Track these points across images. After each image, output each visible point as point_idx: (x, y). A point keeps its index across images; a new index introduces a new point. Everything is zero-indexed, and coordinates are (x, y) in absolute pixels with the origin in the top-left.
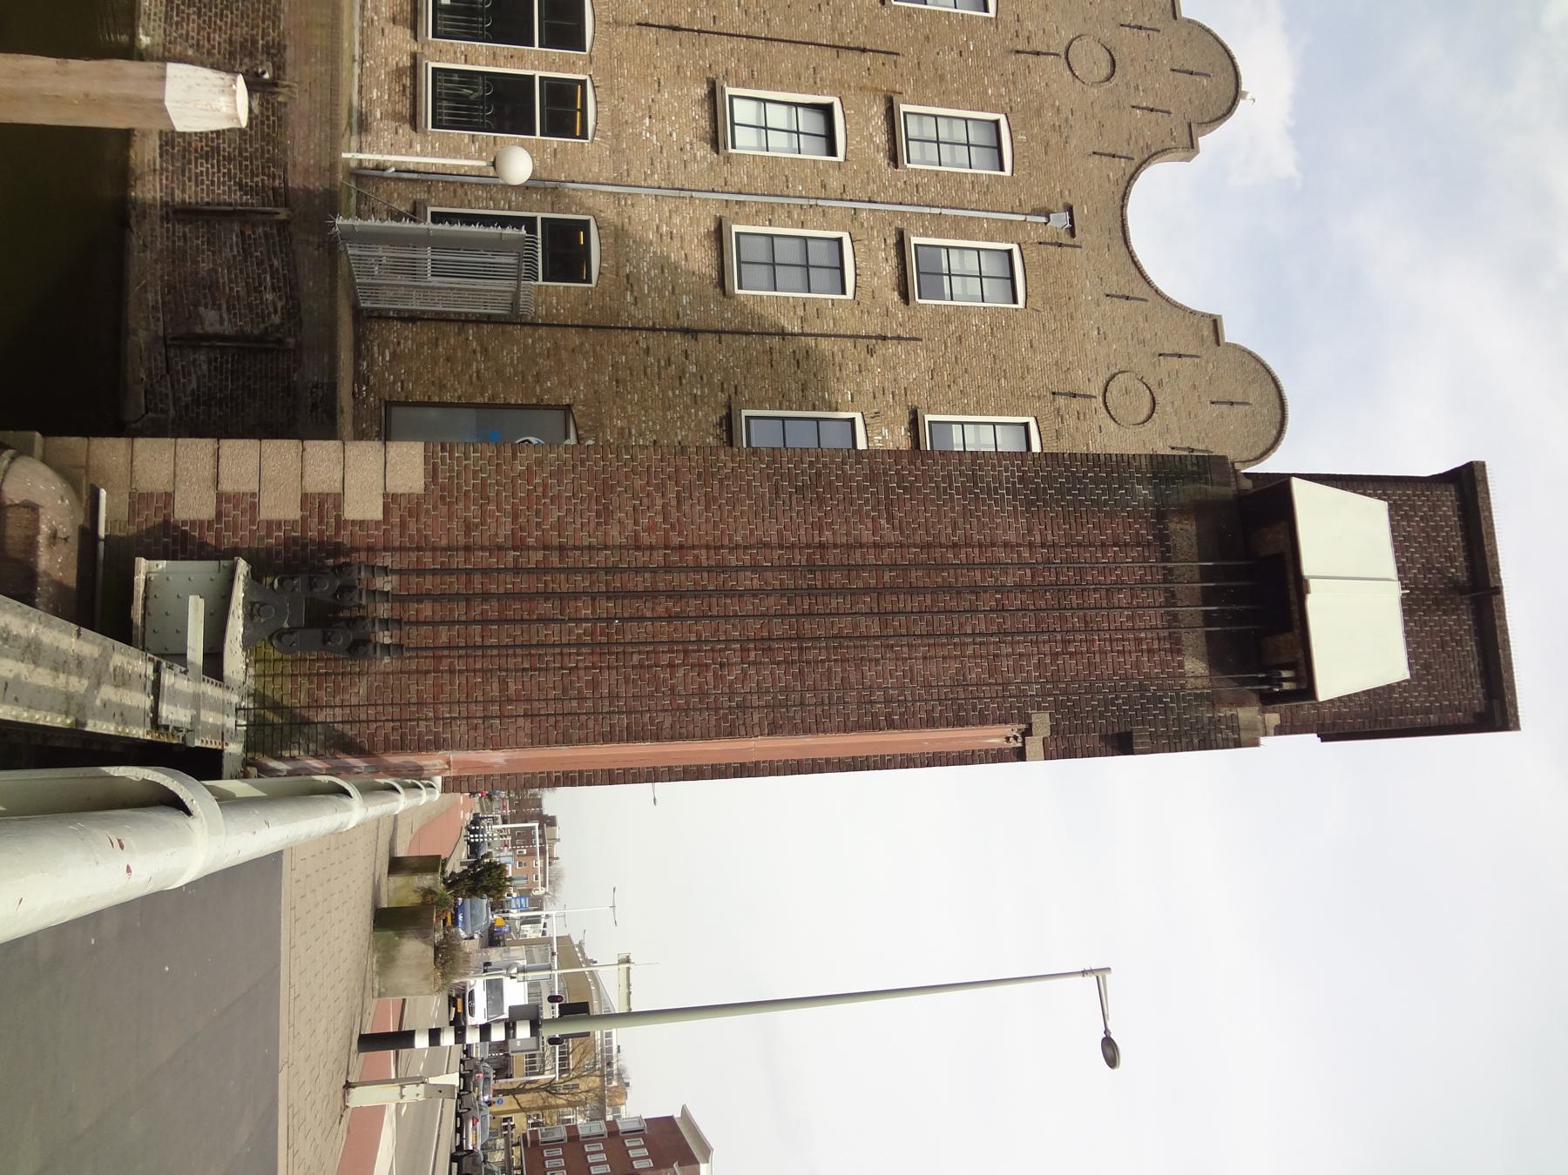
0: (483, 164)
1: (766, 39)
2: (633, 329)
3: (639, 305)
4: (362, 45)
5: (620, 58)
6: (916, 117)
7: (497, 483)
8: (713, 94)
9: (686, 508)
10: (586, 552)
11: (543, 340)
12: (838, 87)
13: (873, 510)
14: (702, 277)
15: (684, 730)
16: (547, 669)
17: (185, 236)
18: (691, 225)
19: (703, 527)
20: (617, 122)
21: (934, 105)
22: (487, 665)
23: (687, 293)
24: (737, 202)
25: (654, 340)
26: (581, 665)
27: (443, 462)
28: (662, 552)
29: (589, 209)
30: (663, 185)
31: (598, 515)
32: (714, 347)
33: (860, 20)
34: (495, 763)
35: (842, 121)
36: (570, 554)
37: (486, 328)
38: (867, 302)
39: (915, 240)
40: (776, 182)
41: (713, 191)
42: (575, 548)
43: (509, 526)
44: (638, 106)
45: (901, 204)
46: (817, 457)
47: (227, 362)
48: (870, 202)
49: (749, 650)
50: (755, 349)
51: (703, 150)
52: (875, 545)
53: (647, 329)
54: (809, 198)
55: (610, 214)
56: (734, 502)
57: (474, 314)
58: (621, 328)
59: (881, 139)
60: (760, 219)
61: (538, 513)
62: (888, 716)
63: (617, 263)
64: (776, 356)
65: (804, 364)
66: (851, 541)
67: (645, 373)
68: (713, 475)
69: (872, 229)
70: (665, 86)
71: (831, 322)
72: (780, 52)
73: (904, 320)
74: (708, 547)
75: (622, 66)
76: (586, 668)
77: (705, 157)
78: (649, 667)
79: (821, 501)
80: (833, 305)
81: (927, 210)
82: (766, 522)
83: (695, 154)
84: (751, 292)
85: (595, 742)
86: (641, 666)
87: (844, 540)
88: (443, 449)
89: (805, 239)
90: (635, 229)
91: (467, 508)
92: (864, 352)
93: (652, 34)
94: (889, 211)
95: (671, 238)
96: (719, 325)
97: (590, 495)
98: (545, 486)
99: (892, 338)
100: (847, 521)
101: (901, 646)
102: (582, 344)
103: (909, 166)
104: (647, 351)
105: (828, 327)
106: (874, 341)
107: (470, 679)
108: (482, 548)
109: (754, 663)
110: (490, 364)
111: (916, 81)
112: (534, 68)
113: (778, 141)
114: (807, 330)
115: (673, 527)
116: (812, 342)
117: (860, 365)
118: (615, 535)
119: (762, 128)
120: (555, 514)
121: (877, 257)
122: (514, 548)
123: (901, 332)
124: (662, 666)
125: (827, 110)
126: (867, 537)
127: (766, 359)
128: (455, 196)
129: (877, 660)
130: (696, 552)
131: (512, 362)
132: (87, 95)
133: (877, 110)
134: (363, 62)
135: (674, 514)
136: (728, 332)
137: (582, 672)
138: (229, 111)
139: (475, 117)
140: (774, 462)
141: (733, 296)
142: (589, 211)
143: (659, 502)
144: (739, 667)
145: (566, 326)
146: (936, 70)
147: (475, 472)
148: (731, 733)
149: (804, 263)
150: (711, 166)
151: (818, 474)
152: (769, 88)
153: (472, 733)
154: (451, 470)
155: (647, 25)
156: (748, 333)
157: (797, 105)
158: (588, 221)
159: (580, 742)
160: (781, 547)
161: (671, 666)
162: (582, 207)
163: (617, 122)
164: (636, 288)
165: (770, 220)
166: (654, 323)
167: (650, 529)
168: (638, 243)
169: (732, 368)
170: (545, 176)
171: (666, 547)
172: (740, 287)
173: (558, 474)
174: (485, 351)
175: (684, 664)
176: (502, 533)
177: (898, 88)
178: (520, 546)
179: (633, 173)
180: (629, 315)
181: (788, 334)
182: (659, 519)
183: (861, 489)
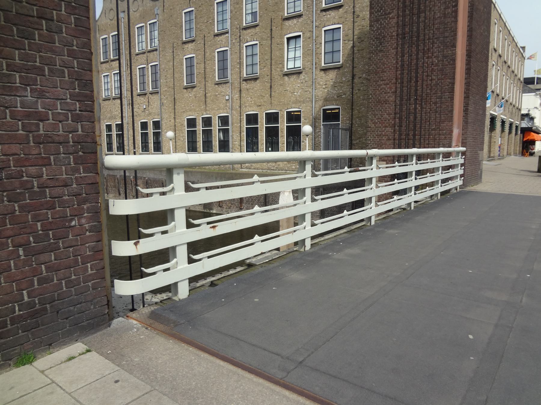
0: (307, 139)
1: (271, 60)
2: (352, 94)
3: (346, 93)
4: (282, 170)
5: (280, 102)
6: (288, 10)
7: (377, 132)
8: (287, 75)
9: (385, 78)
10: (397, 107)
11: (356, 122)
12: (282, 37)
13: (387, 19)
14: (337, 74)
15: (452, 75)
16: (430, 117)
17: (328, 213)
18: (322, 79)
19: (391, 73)
20: (296, 102)
21: (284, 5)
22: (427, 134)
23: (342, 78)
24: (315, 65)
25: (356, 88)
26: (429, 107)
27: (371, 146)
28: (398, 85)
29: (319, 109)
30: (312, 88)
31: (386, 104)
32: (358, 69)
33: (263, 32)
34: (458, 132)
35: (291, 34)
36: (397, 111)
37: (353, 138)
38: (343, 20)
39: (324, 5)
40: (309, 53)
41: (313, 73)
42: (395, 110)
43: (389, 128)
44: (292, 96)
45: (313, 12)
46: (371, 39)
47: (359, 205)
48: (313, 22)
49: (428, 56)
50: (358, 56)
51: (302, 76)
52: (398, 18)
53: (353, 90)
54: (313, 42)
55: (320, 103)
56: (384, 64)
57: (349, 141)
58: (352, 98)
59: (295, 21)
60: (320, 57)
61: (385, 121)
62: (453, 7)
63: (334, 100)
64: (360, 48)
65: (362, 39)
66: (396, 26)
67: (366, 90)
68: (376, 71)
69: (321, 20)
70: (286, 89)
71: (349, 31)
72: (274, 55)
73: (348, 6)
74: (397, 71)
75: (282, 101)
76: (430, 106)
77: (304, 76)
78: (431, 87)
79: (384, 37)
80: (344, 31)
81: (314, 3)
82: (390, 53)
83: (303, 79)
84: (341, 58)
85: (453, 103)
86: (431, 89)
87: (396, 28)
88: (368, 146)
89: (325, 42)
90: (324, 95)
91: (384, 140)
92: (359, 19)
93: (273, 93)
94: (316, 16)
95: (326, 84)
96: (351, 68)
97: (381, 106)
98: (378, 119)
99: (354, 9)
100: (390, 28)
101: (430, 5)
102: (357, 110)
103: (302, 11)
104: (359, 90)
105: (351, 32)
106: (355, 16)
107: (431, 139)
108: (394, 135)
109: (432, 54)
110: (363, 137)
111: (278, 12)
112: (284, 126)
113: (299, 53)
114: (352, 39)
115: (390, 82)
116: (356, 37)
117: (363, 20)
118: (392, 99)
119: (295, 59)
120: (386, 116)
121: (329, 18)
122: (395, 127)
123: (352, 7)
124: (431, 83)
125: (289, 39)
126: (395, 21)
127: (361, 52)
128: (318, 146)
129: (434, 13)
130: (398, 74)
131: (362, 130)
132: (287, 222)
133: (287, 23)
134: (286, 170)
135: (387, 81)
136: (353, 64)
137: (431, 107)
138: (288, 193)
139: (298, 141)
140: (372, 52)
141: (342, 64)
142: (320, 109)
143: (383, 86)
144: (433, 59)
145: (352, 114)
146: (274, 5)
147: (374, 138)
148: (454, 60)
149: (332, 42)
150: (306, 74)
151: (376, 38)
152: (284, 58)
153: (447, 138)
154: (373, 144)
155: (271, 95)
156: (353, 58)
157: (288, 49)
158: (323, 109)
159: (452, 107)
160: (397, 48)
161: (431, 80)
162: (319, 111)
163: (296, 102)
164: (341, 94)
165: (320, 54)
166: (351, 88)
167: (391, 88)
168: (328, 94)
169: (364, 62)
170: (311, 122)
171: (396, 83)
172: (340, 62)
173: (375, 115)
174: (360, 138)
175: (431, 76)
176: (390, 130)
177: (280, 17)
178: (394, 125)
179: (309, 97)
180: (349, 96)
181: (353, 45)
182: (388, 86)
183: (381, 24)
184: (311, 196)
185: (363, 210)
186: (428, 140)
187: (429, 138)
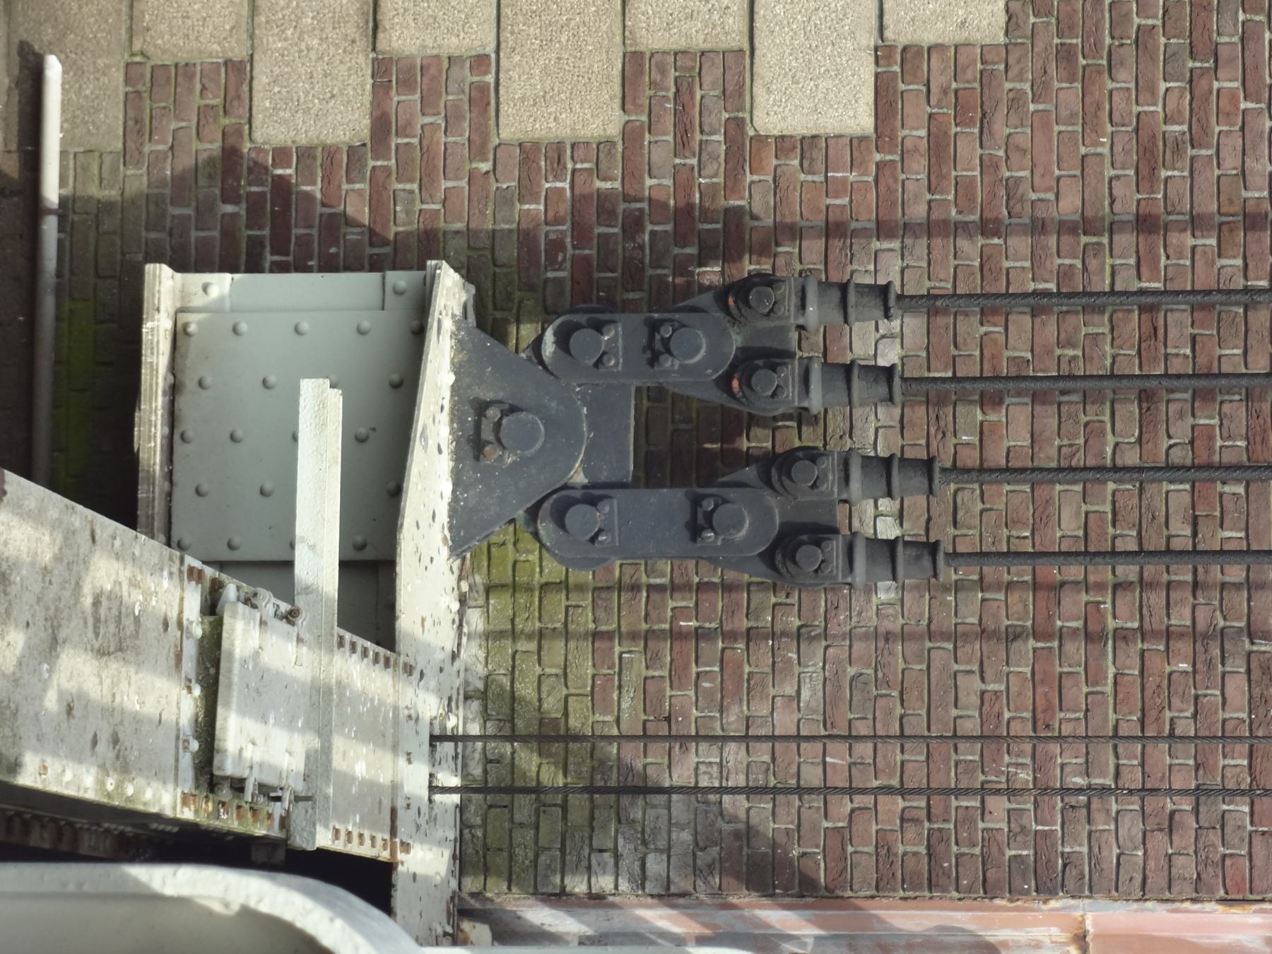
91: (1144, 88)
107: (1157, 664)
108: (1196, 223)
153: (1159, 842)
184: (288, 831)
185: (174, 390)
186: (1143, 633)
187: (1168, 635)
